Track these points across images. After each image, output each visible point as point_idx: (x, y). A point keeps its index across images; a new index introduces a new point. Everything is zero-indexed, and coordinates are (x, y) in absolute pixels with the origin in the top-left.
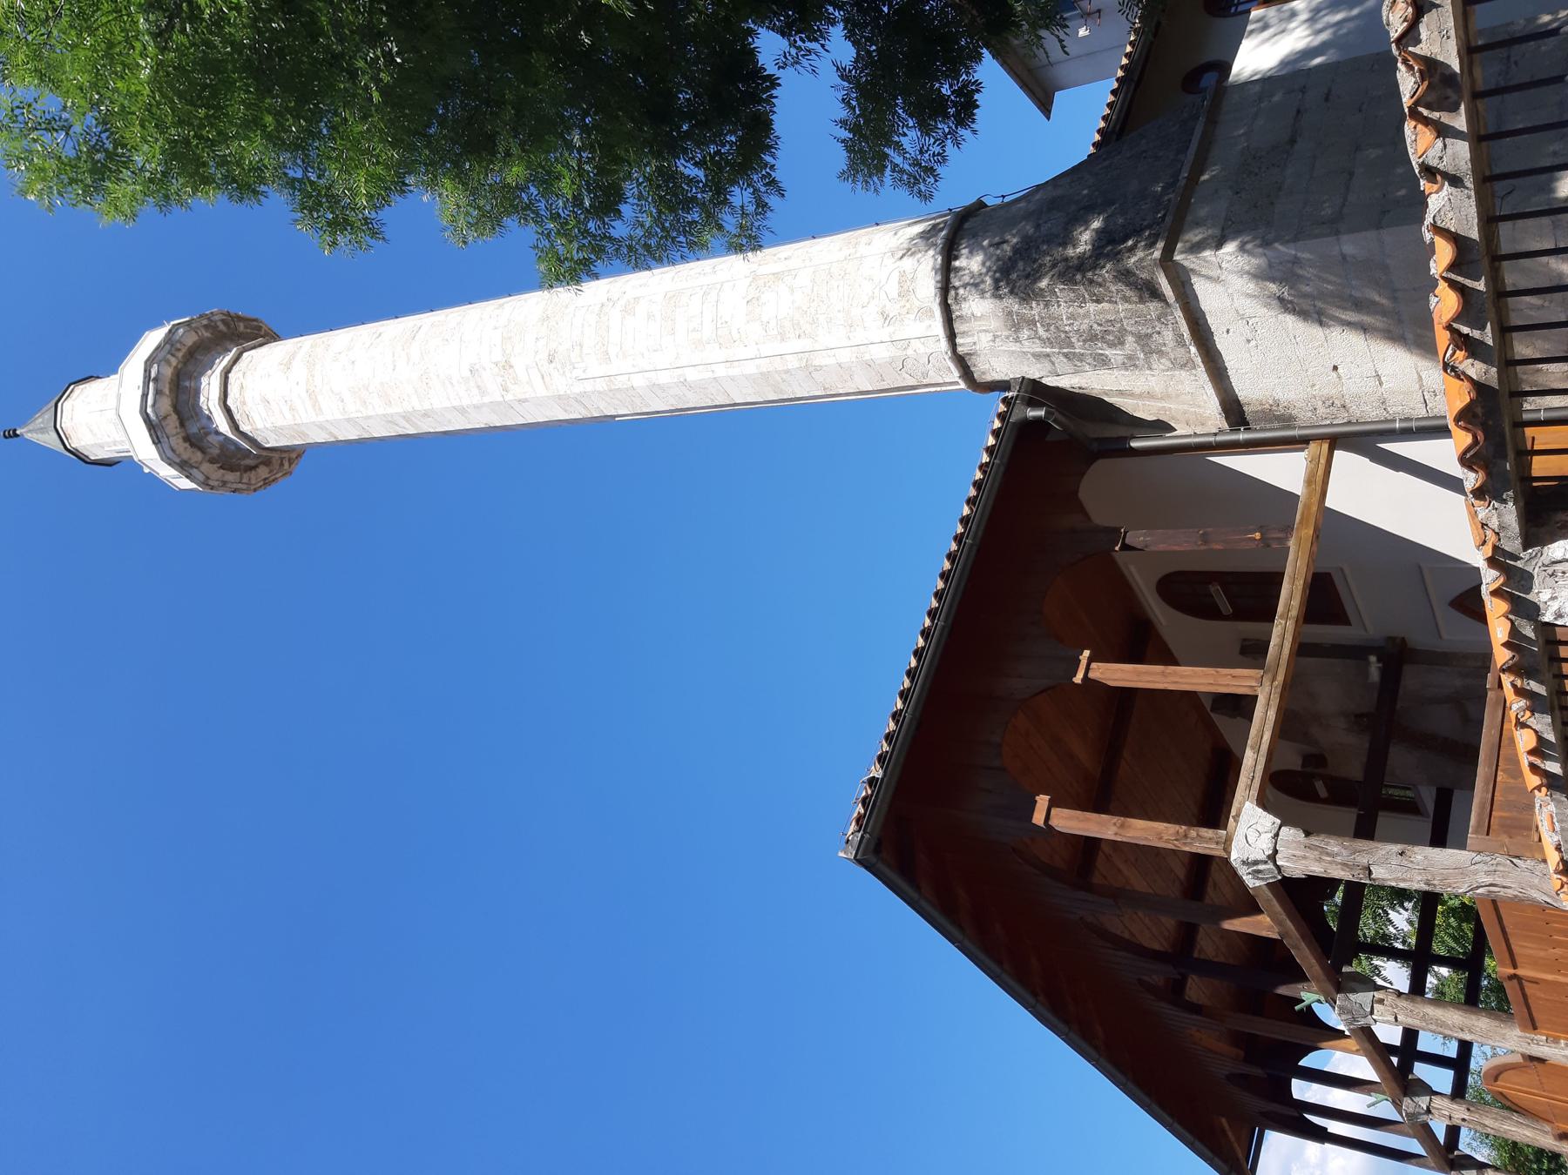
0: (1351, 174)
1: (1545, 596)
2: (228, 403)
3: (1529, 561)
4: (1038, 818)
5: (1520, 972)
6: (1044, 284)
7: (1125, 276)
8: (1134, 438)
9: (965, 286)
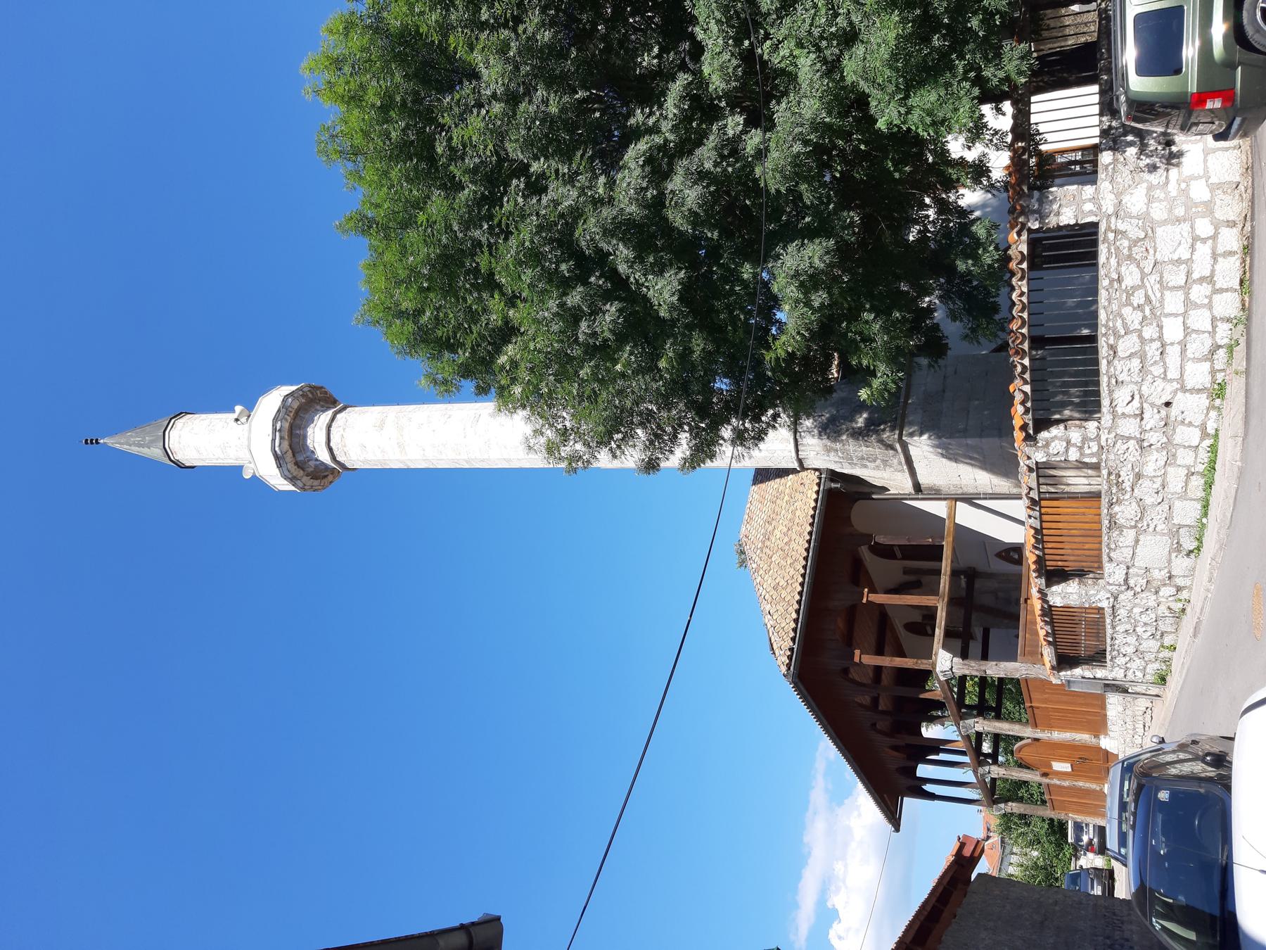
0: (969, 411)
1: (1051, 599)
2: (331, 445)
4: (857, 659)
5: (1033, 705)
6: (844, 437)
7: (881, 441)
8: (873, 493)
9: (804, 432)
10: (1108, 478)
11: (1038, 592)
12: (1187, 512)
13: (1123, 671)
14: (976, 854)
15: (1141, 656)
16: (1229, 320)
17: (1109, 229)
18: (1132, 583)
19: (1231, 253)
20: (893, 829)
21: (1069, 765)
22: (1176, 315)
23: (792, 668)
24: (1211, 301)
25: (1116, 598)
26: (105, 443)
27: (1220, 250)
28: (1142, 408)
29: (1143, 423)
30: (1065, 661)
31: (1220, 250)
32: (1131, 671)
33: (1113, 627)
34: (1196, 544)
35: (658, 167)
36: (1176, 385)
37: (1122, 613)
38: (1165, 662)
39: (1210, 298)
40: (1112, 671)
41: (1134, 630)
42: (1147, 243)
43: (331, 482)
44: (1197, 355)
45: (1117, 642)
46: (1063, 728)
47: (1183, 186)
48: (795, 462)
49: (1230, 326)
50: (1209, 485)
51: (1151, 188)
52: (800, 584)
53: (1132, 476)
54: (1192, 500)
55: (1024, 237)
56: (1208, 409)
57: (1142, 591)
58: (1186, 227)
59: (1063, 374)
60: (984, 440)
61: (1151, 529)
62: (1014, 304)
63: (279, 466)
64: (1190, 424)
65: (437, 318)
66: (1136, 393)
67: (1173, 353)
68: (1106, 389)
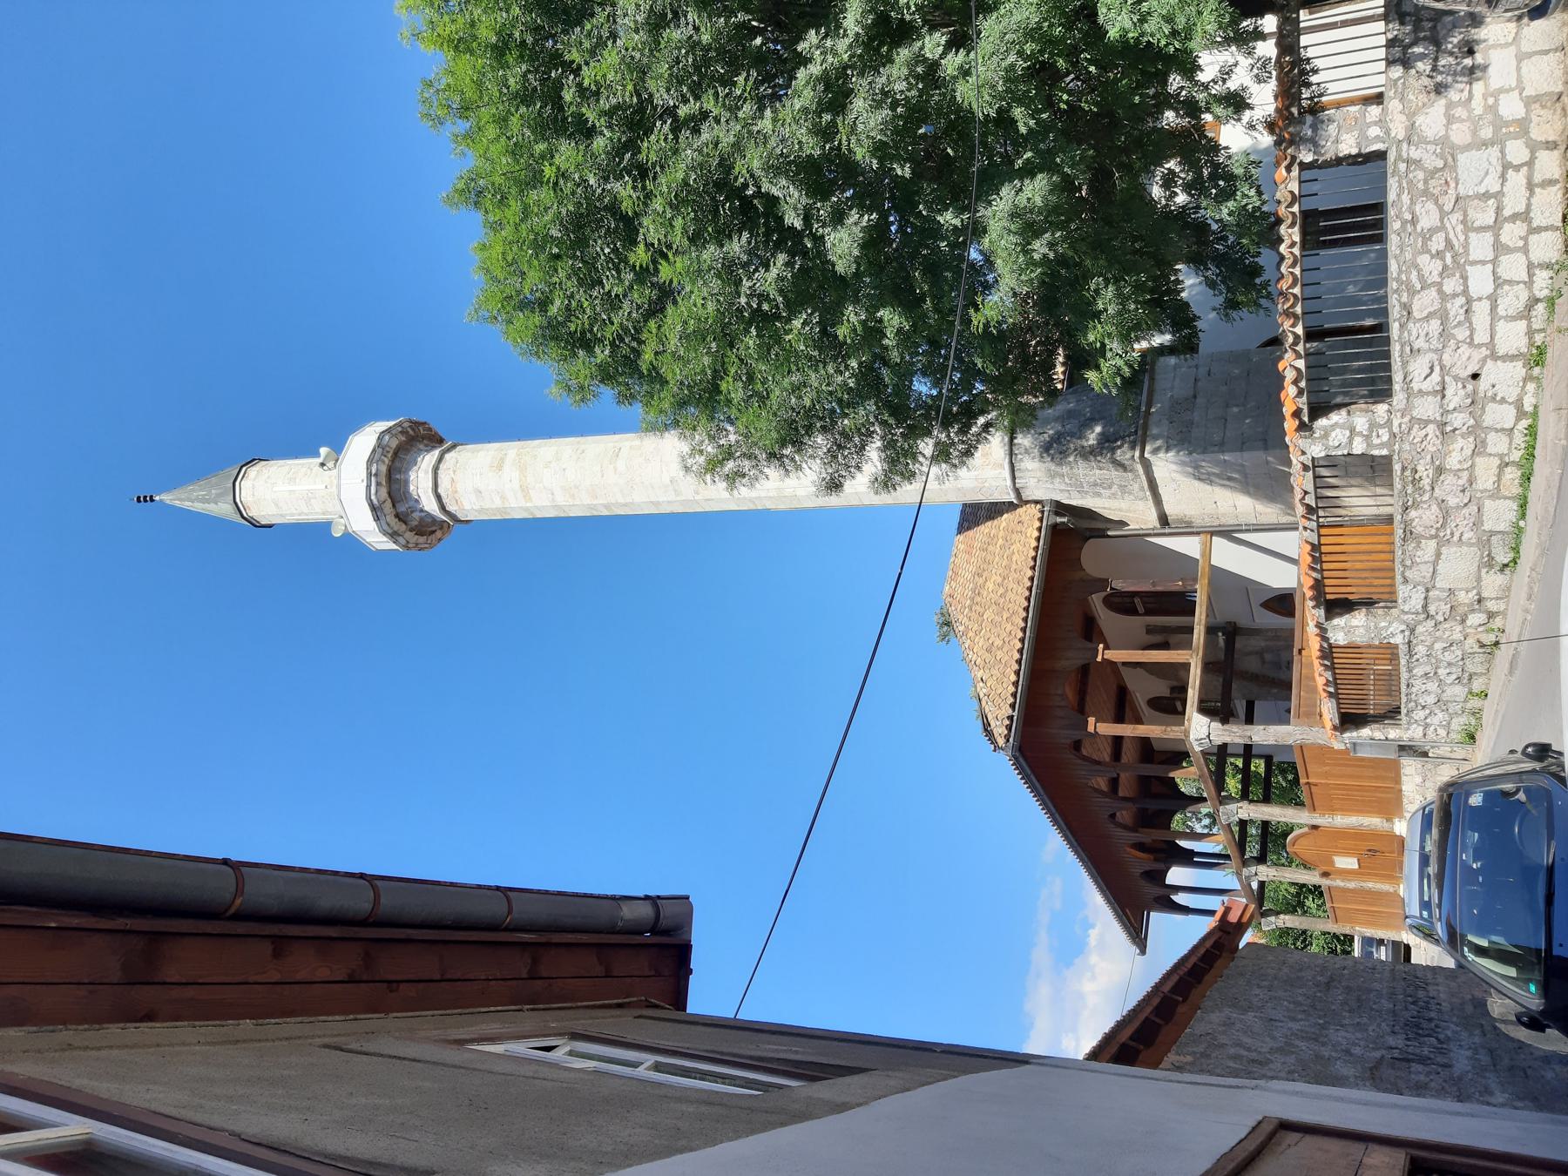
3: (1326, 625)
4: (1091, 729)
5: (1309, 781)
6: (1071, 459)
8: (1108, 529)
10: (1402, 474)
11: (1316, 626)
12: (1500, 514)
13: (1421, 728)
14: (1245, 919)
15: (1444, 708)
16: (1548, 266)
17: (1399, 158)
18: (1432, 609)
19: (1551, 182)
20: (1138, 951)
21: (1356, 860)
22: (1483, 263)
23: (1011, 740)
24: (1526, 244)
25: (1412, 631)
26: (161, 500)
27: (1537, 178)
28: (1443, 382)
29: (1445, 401)
30: (1349, 720)
31: (1537, 178)
32: (1432, 728)
33: (1410, 670)
34: (1511, 555)
35: (836, 93)
36: (1484, 351)
37: (1421, 650)
38: (1474, 714)
39: (1525, 239)
40: (1408, 729)
41: (1436, 673)
42: (1447, 175)
43: (440, 540)
44: (1510, 312)
45: (1414, 690)
46: (1346, 810)
47: (1491, 101)
48: (1011, 493)
49: (1551, 273)
50: (1527, 478)
51: (1450, 106)
52: (1018, 651)
53: (1431, 471)
54: (1506, 498)
55: (1295, 172)
56: (1525, 380)
57: (1445, 620)
58: (1494, 152)
59: (1344, 371)
60: (1246, 455)
61: (1456, 538)
62: (1282, 258)
63: (377, 519)
64: (1503, 401)
65: (568, 308)
66: (1436, 363)
67: (1481, 310)
68: (1398, 359)
